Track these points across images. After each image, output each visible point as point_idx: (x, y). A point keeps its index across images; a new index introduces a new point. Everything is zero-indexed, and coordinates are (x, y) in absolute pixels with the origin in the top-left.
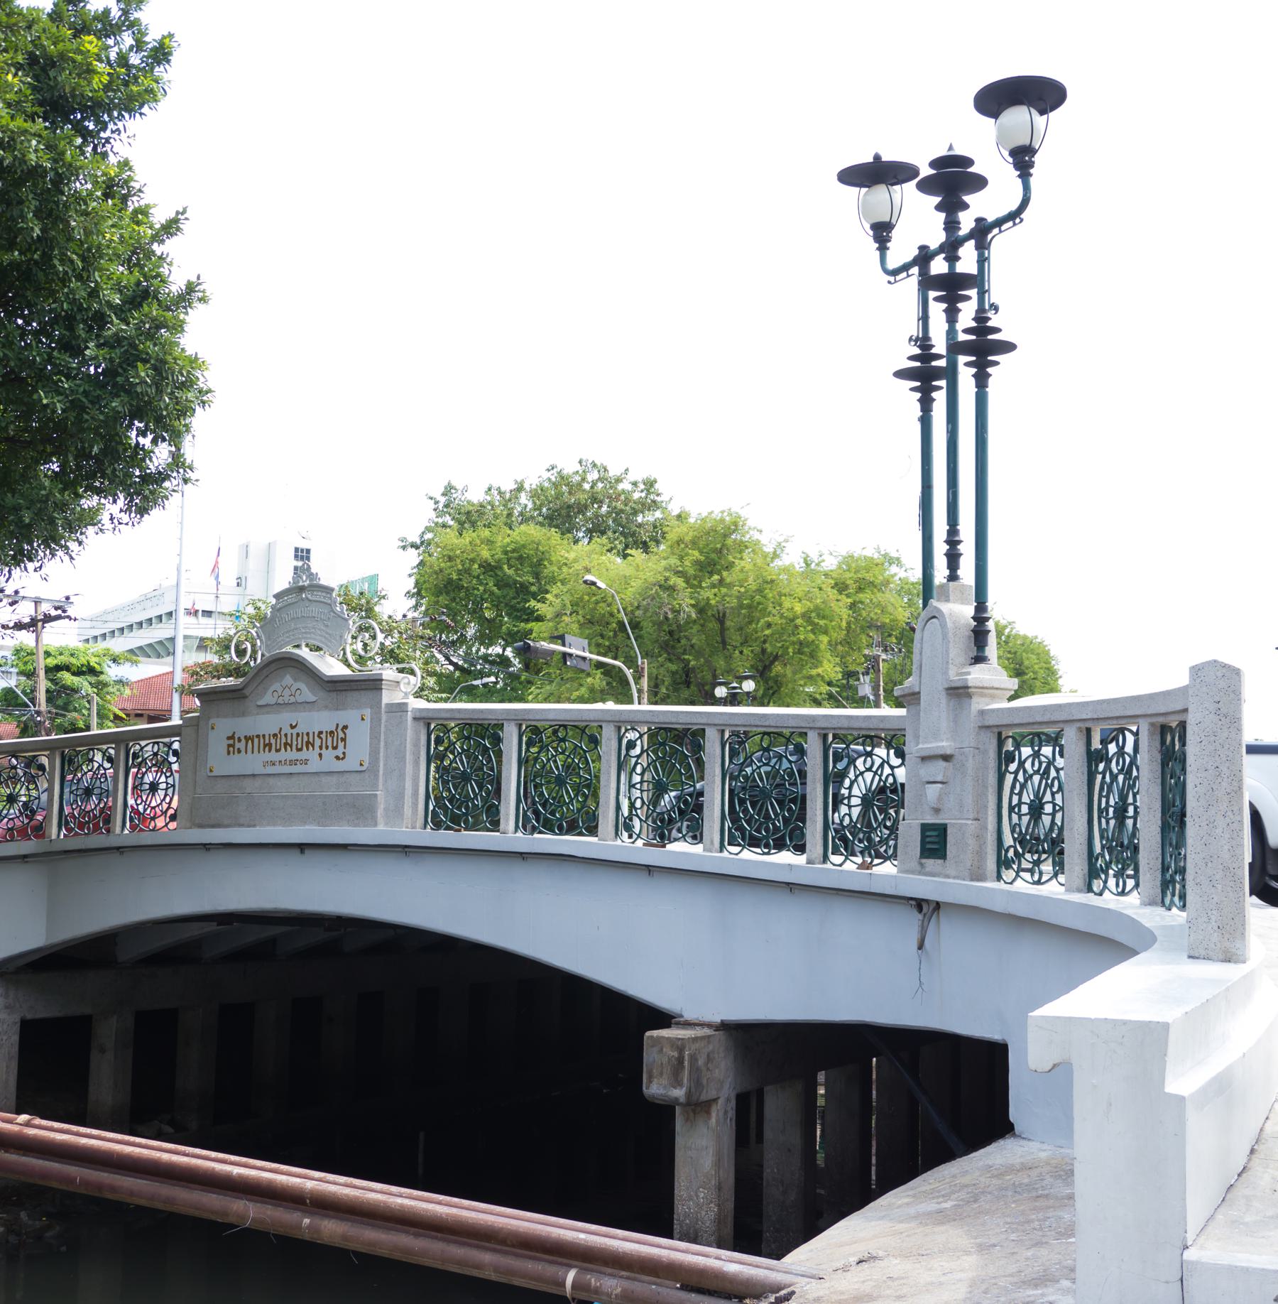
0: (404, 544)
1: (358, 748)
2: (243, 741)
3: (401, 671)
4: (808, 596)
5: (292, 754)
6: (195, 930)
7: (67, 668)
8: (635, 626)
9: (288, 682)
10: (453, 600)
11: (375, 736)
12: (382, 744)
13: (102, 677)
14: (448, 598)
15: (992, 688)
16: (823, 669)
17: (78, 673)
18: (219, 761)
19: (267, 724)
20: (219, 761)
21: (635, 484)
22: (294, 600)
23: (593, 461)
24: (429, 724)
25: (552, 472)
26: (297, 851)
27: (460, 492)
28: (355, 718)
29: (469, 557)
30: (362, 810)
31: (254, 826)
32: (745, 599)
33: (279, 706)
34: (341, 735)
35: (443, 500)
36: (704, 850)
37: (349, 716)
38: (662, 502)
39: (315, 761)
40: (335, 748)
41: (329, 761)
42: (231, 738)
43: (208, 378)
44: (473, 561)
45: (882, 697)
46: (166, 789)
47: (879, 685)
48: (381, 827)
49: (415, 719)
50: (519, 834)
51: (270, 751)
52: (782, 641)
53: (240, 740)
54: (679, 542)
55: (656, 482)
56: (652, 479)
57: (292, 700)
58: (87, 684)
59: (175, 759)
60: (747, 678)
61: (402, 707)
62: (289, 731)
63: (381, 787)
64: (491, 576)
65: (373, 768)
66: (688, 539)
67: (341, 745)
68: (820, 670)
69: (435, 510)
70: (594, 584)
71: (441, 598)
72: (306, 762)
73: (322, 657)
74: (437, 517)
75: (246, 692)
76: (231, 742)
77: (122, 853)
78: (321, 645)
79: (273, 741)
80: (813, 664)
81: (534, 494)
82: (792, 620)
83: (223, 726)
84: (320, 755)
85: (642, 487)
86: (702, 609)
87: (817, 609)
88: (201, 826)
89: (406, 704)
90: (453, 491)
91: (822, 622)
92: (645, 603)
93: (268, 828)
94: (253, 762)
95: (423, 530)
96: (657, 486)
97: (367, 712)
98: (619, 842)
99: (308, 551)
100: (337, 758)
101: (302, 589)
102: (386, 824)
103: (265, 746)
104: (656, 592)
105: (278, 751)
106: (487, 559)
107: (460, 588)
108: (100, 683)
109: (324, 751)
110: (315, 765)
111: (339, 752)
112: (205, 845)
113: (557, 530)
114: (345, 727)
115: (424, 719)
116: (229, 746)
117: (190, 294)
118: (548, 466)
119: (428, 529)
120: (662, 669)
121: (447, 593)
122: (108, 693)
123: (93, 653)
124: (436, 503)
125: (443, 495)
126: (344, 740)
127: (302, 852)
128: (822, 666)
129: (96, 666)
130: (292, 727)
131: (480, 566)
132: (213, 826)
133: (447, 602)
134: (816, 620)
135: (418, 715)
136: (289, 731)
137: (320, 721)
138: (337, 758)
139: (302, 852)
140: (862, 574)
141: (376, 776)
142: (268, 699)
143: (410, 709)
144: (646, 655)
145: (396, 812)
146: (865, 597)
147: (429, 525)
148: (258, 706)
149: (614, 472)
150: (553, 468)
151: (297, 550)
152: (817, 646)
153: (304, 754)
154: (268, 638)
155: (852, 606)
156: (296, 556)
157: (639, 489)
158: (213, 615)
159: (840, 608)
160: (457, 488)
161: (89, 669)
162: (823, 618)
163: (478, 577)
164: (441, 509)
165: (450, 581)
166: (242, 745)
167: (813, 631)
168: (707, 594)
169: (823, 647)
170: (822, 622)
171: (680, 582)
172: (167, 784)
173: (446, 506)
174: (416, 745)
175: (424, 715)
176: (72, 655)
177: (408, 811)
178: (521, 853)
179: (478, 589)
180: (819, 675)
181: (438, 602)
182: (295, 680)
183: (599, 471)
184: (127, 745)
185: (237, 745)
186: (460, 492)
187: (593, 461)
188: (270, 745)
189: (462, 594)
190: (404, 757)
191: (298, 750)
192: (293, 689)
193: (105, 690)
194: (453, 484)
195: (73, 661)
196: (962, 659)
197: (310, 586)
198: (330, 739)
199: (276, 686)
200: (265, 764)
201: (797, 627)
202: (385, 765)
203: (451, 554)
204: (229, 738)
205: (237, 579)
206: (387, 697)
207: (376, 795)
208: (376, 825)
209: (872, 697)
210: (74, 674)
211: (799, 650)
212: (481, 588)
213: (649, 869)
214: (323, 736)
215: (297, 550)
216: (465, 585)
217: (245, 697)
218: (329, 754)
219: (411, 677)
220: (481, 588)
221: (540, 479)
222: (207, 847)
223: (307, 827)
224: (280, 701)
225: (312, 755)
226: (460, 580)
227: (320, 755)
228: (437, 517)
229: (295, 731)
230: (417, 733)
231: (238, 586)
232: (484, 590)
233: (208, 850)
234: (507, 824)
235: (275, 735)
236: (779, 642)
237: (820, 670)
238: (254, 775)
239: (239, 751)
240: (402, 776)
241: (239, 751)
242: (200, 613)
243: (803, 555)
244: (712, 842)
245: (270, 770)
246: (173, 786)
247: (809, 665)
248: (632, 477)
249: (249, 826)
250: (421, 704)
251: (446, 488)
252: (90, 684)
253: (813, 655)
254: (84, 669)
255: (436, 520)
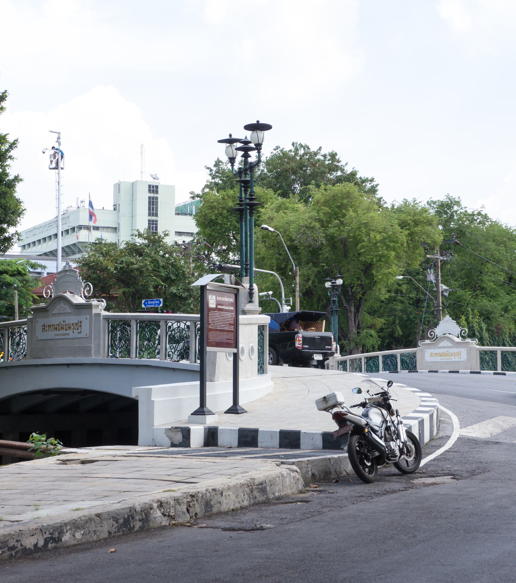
0: (193, 195)
1: (85, 330)
2: (48, 327)
3: (98, 301)
4: (385, 230)
5: (64, 332)
6: (40, 398)
7: (6, 272)
8: (294, 249)
9: (61, 306)
10: (213, 230)
11: (91, 325)
12: (93, 328)
13: (26, 277)
14: (211, 230)
15: (253, 311)
16: (392, 269)
17: (12, 275)
18: (40, 334)
19: (55, 321)
20: (40, 334)
21: (325, 156)
22: (64, 275)
23: (300, 144)
24: (109, 321)
25: (277, 150)
26: (66, 367)
27: (224, 164)
28: (83, 318)
29: (222, 206)
30: (87, 351)
31: (52, 358)
32: (351, 233)
33: (59, 314)
34: (80, 325)
35: (214, 169)
36: (190, 362)
37: (82, 318)
38: (342, 166)
39: (72, 334)
40: (78, 329)
41: (76, 334)
42: (432, 353)
43: (23, 206)
44: (223, 208)
45: (440, 281)
46: (23, 345)
47: (438, 275)
48: (93, 357)
49: (104, 319)
50: (137, 359)
51: (57, 330)
52: (370, 255)
53: (46, 327)
54: (318, 202)
55: (337, 155)
56: (334, 153)
57: (64, 312)
58: (18, 281)
59: (25, 333)
60: (338, 278)
61: (99, 314)
62: (63, 323)
63: (93, 343)
64: (234, 216)
65: (90, 337)
66: (322, 201)
67: (80, 328)
68: (390, 270)
69: (210, 175)
70: (267, 229)
71: (206, 230)
72: (68, 334)
73: (73, 296)
74: (212, 179)
75: (48, 309)
76: (44, 327)
77: (8, 369)
78: (73, 292)
79: (57, 327)
80: (387, 267)
81: (268, 163)
82: (376, 244)
83: (41, 321)
84: (73, 332)
85: (329, 157)
86: (331, 239)
87: (389, 237)
88: (34, 358)
89: (100, 314)
90: (220, 164)
91: (392, 244)
92: (298, 237)
93: (56, 358)
94: (51, 334)
95: (204, 186)
96: (337, 157)
97: (88, 316)
98: (166, 361)
99: (157, 187)
100: (79, 333)
101: (66, 271)
102: (95, 356)
103: (55, 328)
104: (304, 230)
105: (59, 330)
106: (232, 207)
107: (217, 224)
108: (25, 280)
109: (74, 330)
110: (71, 335)
111: (459, 357)
112: (36, 365)
113: (271, 189)
114: (81, 322)
115: (107, 319)
116: (43, 329)
117: (17, 179)
118: (274, 147)
119: (206, 186)
120: (310, 271)
121: (210, 227)
122: (29, 286)
123: (20, 264)
124: (211, 170)
125: (215, 166)
126: (80, 326)
127: (68, 367)
128: (392, 268)
129: (22, 270)
130: (64, 322)
131: (228, 211)
132: (38, 358)
133: (210, 232)
134: (389, 244)
135: (105, 317)
136: (63, 323)
137: (73, 319)
138: (79, 333)
139: (68, 367)
140: (417, 217)
141: (91, 339)
142: (55, 311)
143: (102, 315)
144: (299, 264)
145: (98, 352)
146: (418, 229)
147: (207, 184)
148: (53, 314)
149: (313, 149)
150: (277, 149)
151: (150, 186)
152: (389, 257)
153: (67, 332)
154: (56, 289)
155: (410, 235)
156: (149, 191)
157: (327, 159)
158: (100, 229)
159: (403, 236)
160: (223, 162)
161: (18, 273)
162: (393, 242)
163: (227, 217)
164: (214, 174)
165: (211, 221)
166: (47, 328)
167: (387, 249)
168: (331, 231)
169: (392, 258)
170: (392, 244)
171: (318, 225)
172: (23, 343)
173: (216, 172)
174: (104, 328)
175: (106, 317)
176: (8, 265)
177: (102, 351)
178: (136, 365)
179: (227, 224)
180: (390, 273)
181: (205, 232)
182: (64, 305)
183: (304, 149)
184: (8, 328)
185: (46, 328)
186: (224, 164)
187: (300, 144)
188: (56, 328)
189: (218, 227)
190: (100, 332)
191: (66, 330)
192: (64, 308)
193: (27, 284)
194: (220, 159)
195: (10, 268)
196: (246, 301)
197: (69, 270)
198: (76, 326)
199: (58, 307)
200: (55, 335)
201: (378, 247)
202: (94, 335)
203: (211, 205)
204: (43, 326)
205: (114, 206)
206: (94, 311)
207: (91, 346)
208: (91, 357)
209: (434, 281)
210: (11, 276)
211: (380, 259)
212: (229, 224)
213: (174, 369)
214: (74, 325)
215: (150, 186)
216: (220, 222)
217: (48, 311)
218: (76, 331)
219: (102, 303)
220: (229, 224)
221: (272, 154)
222: (36, 366)
223: (69, 358)
224: (59, 312)
225: (70, 332)
226: (217, 219)
227: (73, 332)
228: (212, 179)
229: (65, 323)
230: (104, 324)
231: (114, 210)
232: (231, 225)
233: (37, 367)
234: (133, 355)
235: (58, 325)
236: (369, 256)
237: (390, 270)
238: (52, 339)
239: (46, 331)
240: (99, 339)
241: (46, 331)
242: (92, 228)
243: (405, 201)
244: (192, 360)
245: (57, 337)
246: (25, 343)
247: (385, 267)
248: (323, 152)
249: (50, 358)
250: (107, 313)
251: (216, 162)
252: (19, 281)
253: (387, 262)
254: (16, 273)
255: (211, 181)
